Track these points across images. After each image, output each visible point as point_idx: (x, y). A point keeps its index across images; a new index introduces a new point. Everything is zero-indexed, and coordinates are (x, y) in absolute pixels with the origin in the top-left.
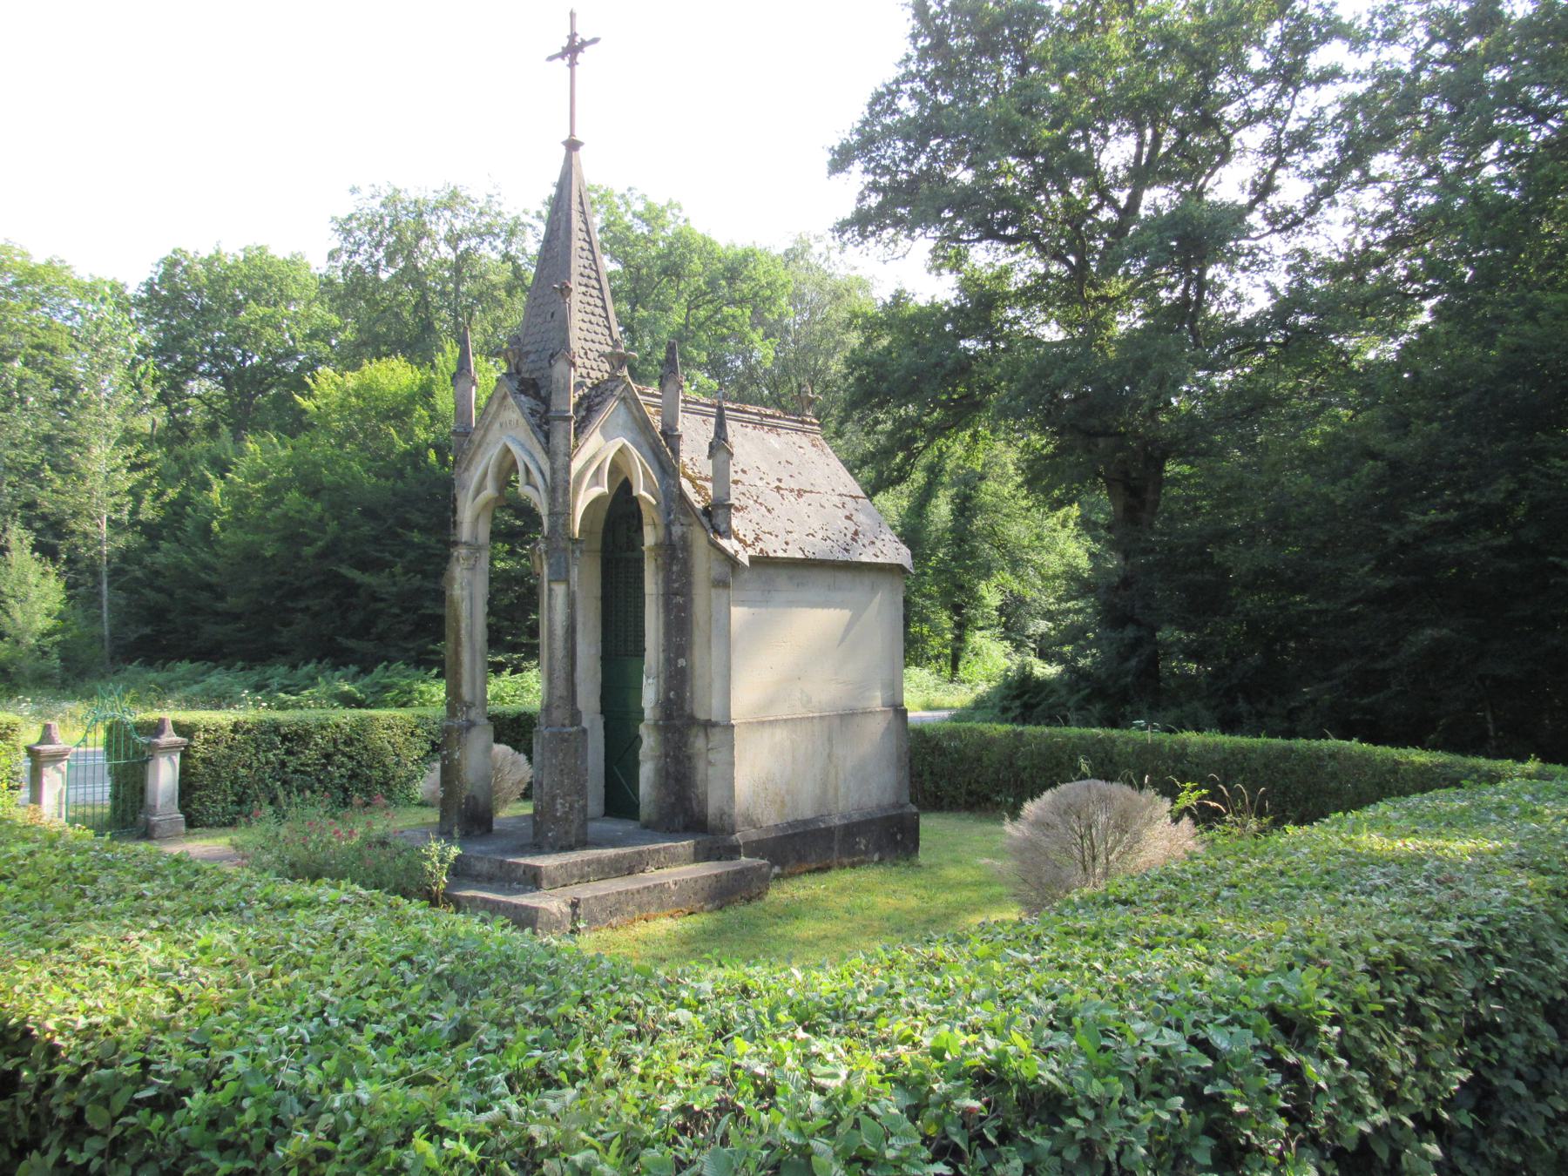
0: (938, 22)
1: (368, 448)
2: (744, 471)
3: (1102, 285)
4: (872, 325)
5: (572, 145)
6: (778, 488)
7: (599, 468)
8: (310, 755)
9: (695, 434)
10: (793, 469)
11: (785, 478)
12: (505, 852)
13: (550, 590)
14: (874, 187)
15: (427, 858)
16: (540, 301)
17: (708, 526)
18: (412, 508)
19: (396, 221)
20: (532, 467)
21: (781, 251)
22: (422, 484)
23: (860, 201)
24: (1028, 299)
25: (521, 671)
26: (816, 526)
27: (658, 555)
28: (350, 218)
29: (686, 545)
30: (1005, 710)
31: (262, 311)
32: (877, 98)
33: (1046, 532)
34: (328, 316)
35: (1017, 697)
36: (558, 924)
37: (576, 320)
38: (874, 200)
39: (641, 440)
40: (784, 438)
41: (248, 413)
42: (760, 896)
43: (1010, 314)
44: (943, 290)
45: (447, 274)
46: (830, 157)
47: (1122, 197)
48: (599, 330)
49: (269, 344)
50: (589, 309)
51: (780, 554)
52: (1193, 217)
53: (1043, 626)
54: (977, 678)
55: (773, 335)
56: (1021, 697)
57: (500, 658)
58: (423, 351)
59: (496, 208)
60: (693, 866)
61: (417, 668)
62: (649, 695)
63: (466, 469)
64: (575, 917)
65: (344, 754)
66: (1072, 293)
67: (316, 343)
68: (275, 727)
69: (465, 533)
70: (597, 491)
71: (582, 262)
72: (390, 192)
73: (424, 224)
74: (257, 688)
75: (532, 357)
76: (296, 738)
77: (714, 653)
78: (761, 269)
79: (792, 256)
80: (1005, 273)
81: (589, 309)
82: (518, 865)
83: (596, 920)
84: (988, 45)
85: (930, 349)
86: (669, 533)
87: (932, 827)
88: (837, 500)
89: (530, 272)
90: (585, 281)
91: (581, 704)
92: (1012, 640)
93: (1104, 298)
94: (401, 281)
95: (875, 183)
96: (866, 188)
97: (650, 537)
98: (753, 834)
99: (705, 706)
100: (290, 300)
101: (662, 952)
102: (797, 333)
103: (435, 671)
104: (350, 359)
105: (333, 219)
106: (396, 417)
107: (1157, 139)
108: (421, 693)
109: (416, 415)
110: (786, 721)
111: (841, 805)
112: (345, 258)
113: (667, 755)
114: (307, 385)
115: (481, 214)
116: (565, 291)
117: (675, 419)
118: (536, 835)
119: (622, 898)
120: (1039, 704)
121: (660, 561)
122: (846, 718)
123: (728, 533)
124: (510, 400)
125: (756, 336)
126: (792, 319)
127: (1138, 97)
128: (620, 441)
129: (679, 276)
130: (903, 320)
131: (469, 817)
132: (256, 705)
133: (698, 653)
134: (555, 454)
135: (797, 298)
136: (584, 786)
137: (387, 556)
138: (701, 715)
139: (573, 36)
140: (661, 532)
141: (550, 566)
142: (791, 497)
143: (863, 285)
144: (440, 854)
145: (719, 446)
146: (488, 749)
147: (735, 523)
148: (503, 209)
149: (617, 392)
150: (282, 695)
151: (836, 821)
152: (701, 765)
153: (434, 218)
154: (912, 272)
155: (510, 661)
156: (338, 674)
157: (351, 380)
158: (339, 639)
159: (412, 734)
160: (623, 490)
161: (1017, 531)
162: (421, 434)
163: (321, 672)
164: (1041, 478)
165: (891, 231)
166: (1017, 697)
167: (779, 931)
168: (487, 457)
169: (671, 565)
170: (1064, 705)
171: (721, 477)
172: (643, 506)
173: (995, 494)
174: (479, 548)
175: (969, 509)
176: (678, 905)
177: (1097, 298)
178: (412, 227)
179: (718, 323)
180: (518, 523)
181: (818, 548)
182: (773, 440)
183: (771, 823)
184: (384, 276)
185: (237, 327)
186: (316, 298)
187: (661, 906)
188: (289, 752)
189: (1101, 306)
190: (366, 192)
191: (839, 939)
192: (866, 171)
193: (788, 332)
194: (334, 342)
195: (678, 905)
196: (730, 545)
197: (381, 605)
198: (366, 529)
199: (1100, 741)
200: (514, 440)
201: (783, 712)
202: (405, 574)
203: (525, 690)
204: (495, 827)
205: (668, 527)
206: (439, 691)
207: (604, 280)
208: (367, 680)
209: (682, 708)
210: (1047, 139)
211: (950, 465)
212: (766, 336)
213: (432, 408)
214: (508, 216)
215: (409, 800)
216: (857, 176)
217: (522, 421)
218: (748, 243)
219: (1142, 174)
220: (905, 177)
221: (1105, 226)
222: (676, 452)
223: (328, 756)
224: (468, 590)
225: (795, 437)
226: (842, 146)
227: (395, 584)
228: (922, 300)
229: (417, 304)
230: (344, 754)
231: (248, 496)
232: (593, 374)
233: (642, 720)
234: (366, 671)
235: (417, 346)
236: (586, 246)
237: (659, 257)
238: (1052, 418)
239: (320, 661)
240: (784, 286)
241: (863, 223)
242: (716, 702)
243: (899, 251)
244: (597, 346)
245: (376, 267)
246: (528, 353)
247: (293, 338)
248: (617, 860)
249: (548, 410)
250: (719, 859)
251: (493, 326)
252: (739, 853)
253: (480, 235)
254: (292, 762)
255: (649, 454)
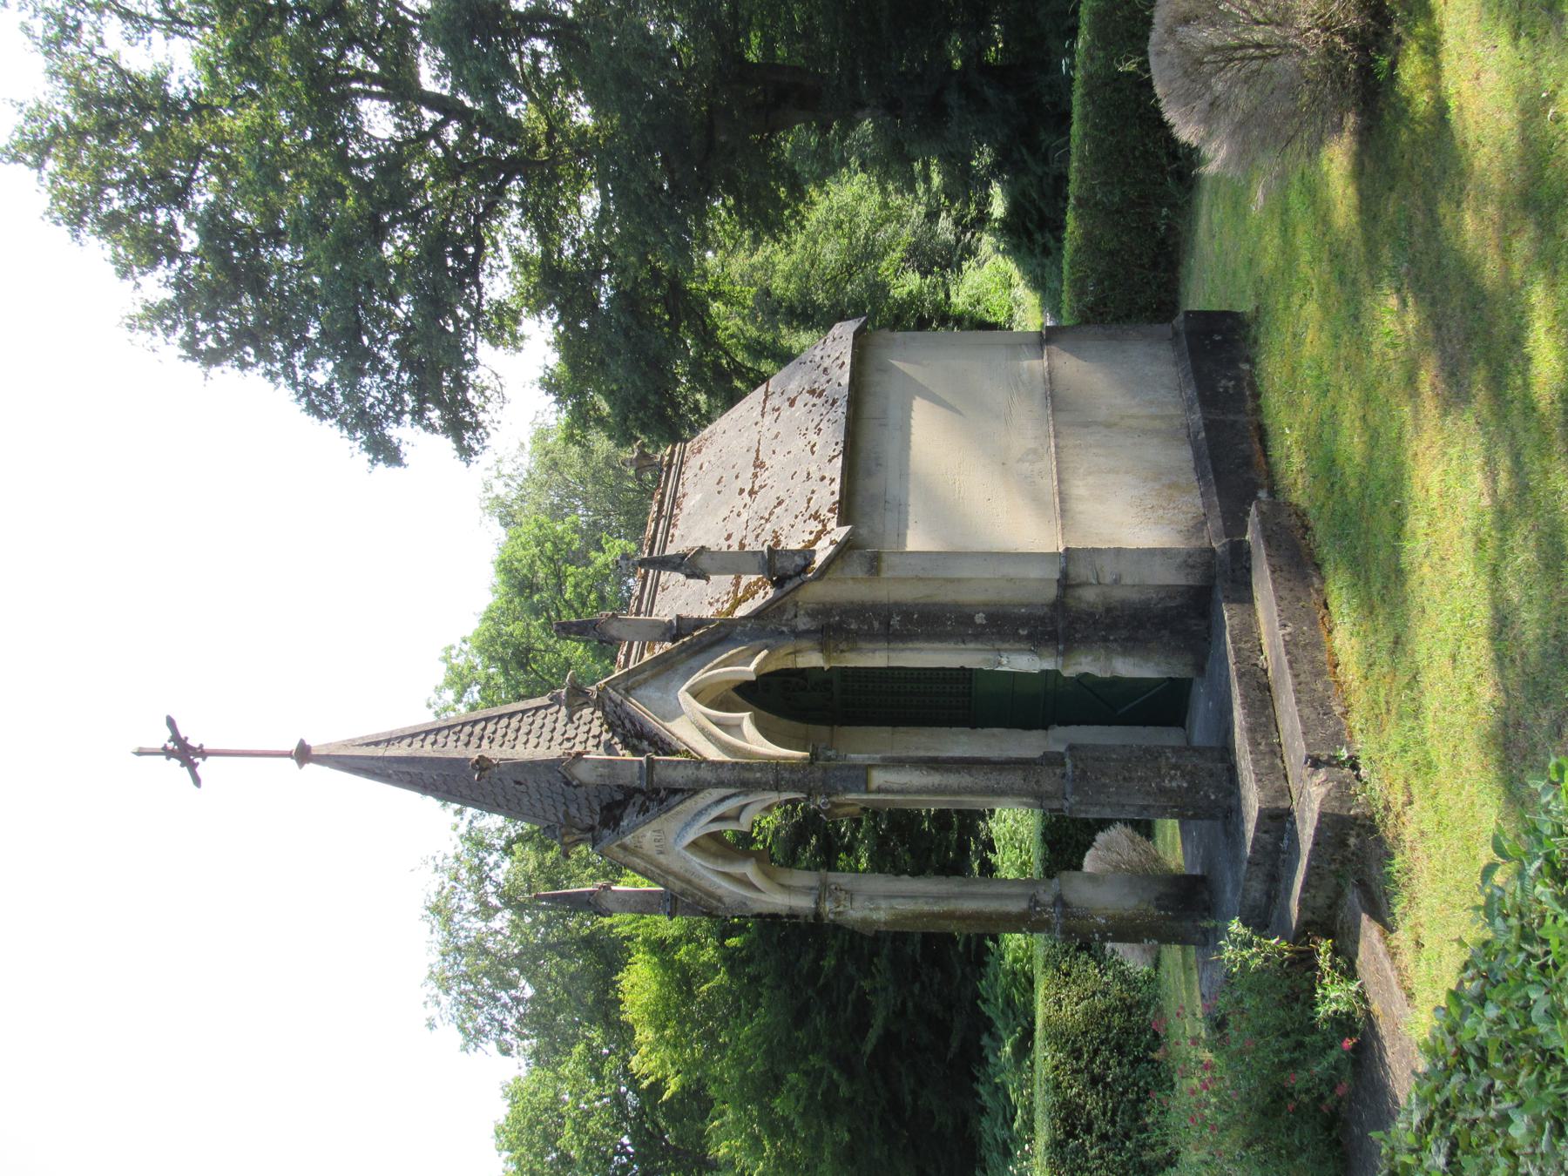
0: (225, 336)
1: (725, 1016)
2: (729, 537)
3: (534, 138)
4: (582, 418)
5: (303, 754)
6: (752, 493)
7: (717, 724)
8: (1092, 1103)
9: (681, 598)
10: (728, 475)
11: (739, 484)
12: (1236, 859)
13: (879, 790)
14: (418, 414)
15: (1245, 964)
16: (501, 799)
17: (797, 581)
18: (792, 967)
19: (466, 977)
20: (716, 812)
21: (502, 530)
22: (766, 953)
23: (435, 430)
24: (552, 229)
25: (991, 840)
26: (801, 442)
27: (836, 649)
28: (462, 1029)
29: (823, 611)
30: (1046, 251)
31: (568, 1131)
32: (314, 409)
33: (833, 217)
34: (576, 1057)
35: (1030, 235)
36: (1342, 785)
37: (523, 753)
38: (434, 415)
39: (682, 669)
40: (689, 488)
41: (687, 1153)
42: (1301, 515)
43: (569, 252)
44: (540, 337)
45: (528, 920)
46: (381, 464)
47: (429, 116)
48: (538, 722)
49: (605, 1125)
50: (511, 735)
51: (836, 486)
52: (447, 19)
53: (945, 224)
54: (1006, 300)
55: (598, 541)
56: (1030, 235)
57: (976, 866)
58: (615, 948)
59: (450, 861)
60: (1259, 605)
61: (985, 964)
62: (1023, 662)
63: (720, 900)
64: (1333, 762)
65: (1092, 1061)
66: (542, 170)
67: (606, 1071)
68: (1056, 1146)
69: (804, 903)
70: (748, 727)
71: (451, 744)
72: (432, 984)
73: (470, 945)
74: (1007, 1154)
75: (573, 811)
76: (1070, 1120)
77: (965, 574)
78: (520, 553)
79: (508, 518)
80: (522, 260)
81: (511, 735)
82: (1256, 839)
83: (1338, 733)
84: (253, 278)
85: (609, 344)
86: (806, 633)
87: (1202, 292)
88: (769, 418)
89: (522, 826)
90: (475, 740)
91: (1035, 753)
92: (962, 258)
93: (549, 136)
94: (534, 975)
95: (413, 413)
96: (419, 423)
97: (812, 659)
98: (1215, 524)
99: (1039, 587)
100: (556, 1099)
101: (1386, 642)
102: (596, 511)
103: (990, 944)
104: (622, 1034)
105: (465, 1049)
106: (688, 983)
107: (360, 76)
108: (1016, 960)
109: (686, 959)
110: (1060, 481)
111: (1172, 411)
112: (507, 1036)
113: (1105, 639)
114: (652, 1084)
115: (456, 879)
116: (483, 764)
117: (657, 624)
118: (1213, 817)
119: (1305, 698)
120: (1039, 210)
121: (843, 646)
122: (1057, 402)
123: (807, 553)
124: (628, 840)
125: (600, 559)
126: (581, 517)
127: (308, 94)
128: (683, 696)
129: (529, 649)
130: (574, 378)
131: (1185, 908)
132: (1026, 1157)
133: (966, 596)
134: (697, 780)
135: (556, 513)
136: (1147, 750)
137: (852, 996)
138: (1051, 593)
139: (203, 753)
140: (805, 644)
141: (847, 790)
142: (764, 476)
143: (542, 435)
144: (1239, 946)
145: (693, 565)
146: (1093, 878)
147: (794, 545)
148: (451, 853)
149: (618, 698)
150: (1016, 1125)
151: (1197, 416)
152: (1118, 594)
153: (463, 934)
154: (519, 375)
155: (978, 854)
156: (991, 1059)
157: (645, 1034)
158: (950, 1056)
159: (1067, 974)
160: (751, 694)
161: (831, 253)
162: (709, 954)
163: (989, 1078)
164: (766, 216)
165: (471, 394)
166: (1030, 235)
167: (1353, 484)
168: (704, 872)
169: (849, 631)
170: (1041, 179)
171: (733, 562)
172: (771, 668)
173: (787, 279)
174: (825, 885)
175: (805, 308)
176: (1314, 623)
177: (549, 144)
178: (471, 959)
179: (584, 604)
180: (813, 841)
181: (831, 438)
182: (691, 502)
183: (1199, 501)
184: (529, 992)
185: (585, 1160)
186: (554, 1070)
187: (1317, 645)
188: (1088, 1129)
189: (558, 139)
190: (433, 1011)
191: (1367, 399)
192: (398, 421)
193: (595, 523)
194: (605, 1051)
195: (1314, 623)
196: (823, 551)
197: (910, 1004)
198: (820, 1021)
199: (1089, 94)
200: (679, 836)
201: (1049, 484)
202: (873, 976)
203: (1014, 829)
204: (1198, 871)
205: (797, 635)
206: (1014, 942)
207: (475, 715)
208: (999, 1024)
209: (1042, 619)
210: (357, 200)
211: (752, 331)
212: (601, 549)
213: (677, 941)
214: (460, 848)
215: (1150, 980)
216: (403, 433)
217: (655, 824)
218: (491, 569)
219: (400, 88)
220: (405, 376)
221: (465, 136)
222: (700, 623)
223: (1095, 1081)
224: (876, 900)
225: (688, 474)
226: (368, 450)
227: (885, 989)
228: (554, 359)
229: (562, 956)
230: (1092, 1061)
231: (780, 1156)
232: (595, 730)
233: (1057, 672)
234: (988, 1025)
235: (608, 957)
236: (431, 738)
237: (506, 672)
238: (694, 195)
239: (977, 1079)
240: (540, 527)
241: (461, 426)
242: (1034, 572)
243: (494, 384)
244: (559, 725)
245: (518, 1001)
246: (566, 814)
247: (600, 1098)
248: (1248, 705)
249: (639, 790)
250: (1249, 570)
251: (586, 867)
252: (1242, 542)
253: (481, 880)
254: (1101, 1125)
255: (702, 657)
